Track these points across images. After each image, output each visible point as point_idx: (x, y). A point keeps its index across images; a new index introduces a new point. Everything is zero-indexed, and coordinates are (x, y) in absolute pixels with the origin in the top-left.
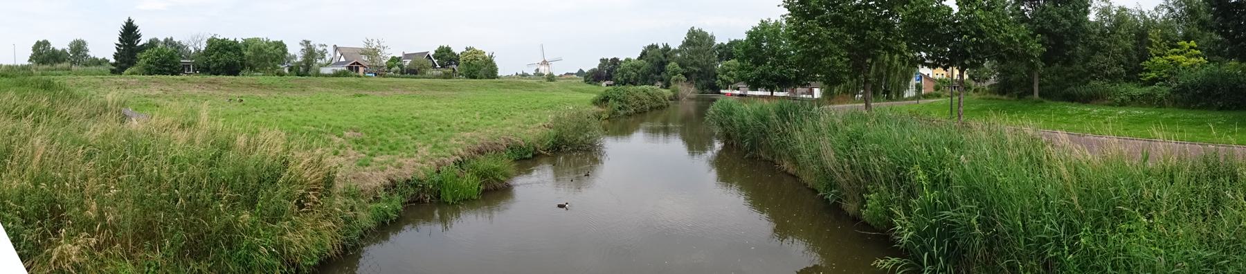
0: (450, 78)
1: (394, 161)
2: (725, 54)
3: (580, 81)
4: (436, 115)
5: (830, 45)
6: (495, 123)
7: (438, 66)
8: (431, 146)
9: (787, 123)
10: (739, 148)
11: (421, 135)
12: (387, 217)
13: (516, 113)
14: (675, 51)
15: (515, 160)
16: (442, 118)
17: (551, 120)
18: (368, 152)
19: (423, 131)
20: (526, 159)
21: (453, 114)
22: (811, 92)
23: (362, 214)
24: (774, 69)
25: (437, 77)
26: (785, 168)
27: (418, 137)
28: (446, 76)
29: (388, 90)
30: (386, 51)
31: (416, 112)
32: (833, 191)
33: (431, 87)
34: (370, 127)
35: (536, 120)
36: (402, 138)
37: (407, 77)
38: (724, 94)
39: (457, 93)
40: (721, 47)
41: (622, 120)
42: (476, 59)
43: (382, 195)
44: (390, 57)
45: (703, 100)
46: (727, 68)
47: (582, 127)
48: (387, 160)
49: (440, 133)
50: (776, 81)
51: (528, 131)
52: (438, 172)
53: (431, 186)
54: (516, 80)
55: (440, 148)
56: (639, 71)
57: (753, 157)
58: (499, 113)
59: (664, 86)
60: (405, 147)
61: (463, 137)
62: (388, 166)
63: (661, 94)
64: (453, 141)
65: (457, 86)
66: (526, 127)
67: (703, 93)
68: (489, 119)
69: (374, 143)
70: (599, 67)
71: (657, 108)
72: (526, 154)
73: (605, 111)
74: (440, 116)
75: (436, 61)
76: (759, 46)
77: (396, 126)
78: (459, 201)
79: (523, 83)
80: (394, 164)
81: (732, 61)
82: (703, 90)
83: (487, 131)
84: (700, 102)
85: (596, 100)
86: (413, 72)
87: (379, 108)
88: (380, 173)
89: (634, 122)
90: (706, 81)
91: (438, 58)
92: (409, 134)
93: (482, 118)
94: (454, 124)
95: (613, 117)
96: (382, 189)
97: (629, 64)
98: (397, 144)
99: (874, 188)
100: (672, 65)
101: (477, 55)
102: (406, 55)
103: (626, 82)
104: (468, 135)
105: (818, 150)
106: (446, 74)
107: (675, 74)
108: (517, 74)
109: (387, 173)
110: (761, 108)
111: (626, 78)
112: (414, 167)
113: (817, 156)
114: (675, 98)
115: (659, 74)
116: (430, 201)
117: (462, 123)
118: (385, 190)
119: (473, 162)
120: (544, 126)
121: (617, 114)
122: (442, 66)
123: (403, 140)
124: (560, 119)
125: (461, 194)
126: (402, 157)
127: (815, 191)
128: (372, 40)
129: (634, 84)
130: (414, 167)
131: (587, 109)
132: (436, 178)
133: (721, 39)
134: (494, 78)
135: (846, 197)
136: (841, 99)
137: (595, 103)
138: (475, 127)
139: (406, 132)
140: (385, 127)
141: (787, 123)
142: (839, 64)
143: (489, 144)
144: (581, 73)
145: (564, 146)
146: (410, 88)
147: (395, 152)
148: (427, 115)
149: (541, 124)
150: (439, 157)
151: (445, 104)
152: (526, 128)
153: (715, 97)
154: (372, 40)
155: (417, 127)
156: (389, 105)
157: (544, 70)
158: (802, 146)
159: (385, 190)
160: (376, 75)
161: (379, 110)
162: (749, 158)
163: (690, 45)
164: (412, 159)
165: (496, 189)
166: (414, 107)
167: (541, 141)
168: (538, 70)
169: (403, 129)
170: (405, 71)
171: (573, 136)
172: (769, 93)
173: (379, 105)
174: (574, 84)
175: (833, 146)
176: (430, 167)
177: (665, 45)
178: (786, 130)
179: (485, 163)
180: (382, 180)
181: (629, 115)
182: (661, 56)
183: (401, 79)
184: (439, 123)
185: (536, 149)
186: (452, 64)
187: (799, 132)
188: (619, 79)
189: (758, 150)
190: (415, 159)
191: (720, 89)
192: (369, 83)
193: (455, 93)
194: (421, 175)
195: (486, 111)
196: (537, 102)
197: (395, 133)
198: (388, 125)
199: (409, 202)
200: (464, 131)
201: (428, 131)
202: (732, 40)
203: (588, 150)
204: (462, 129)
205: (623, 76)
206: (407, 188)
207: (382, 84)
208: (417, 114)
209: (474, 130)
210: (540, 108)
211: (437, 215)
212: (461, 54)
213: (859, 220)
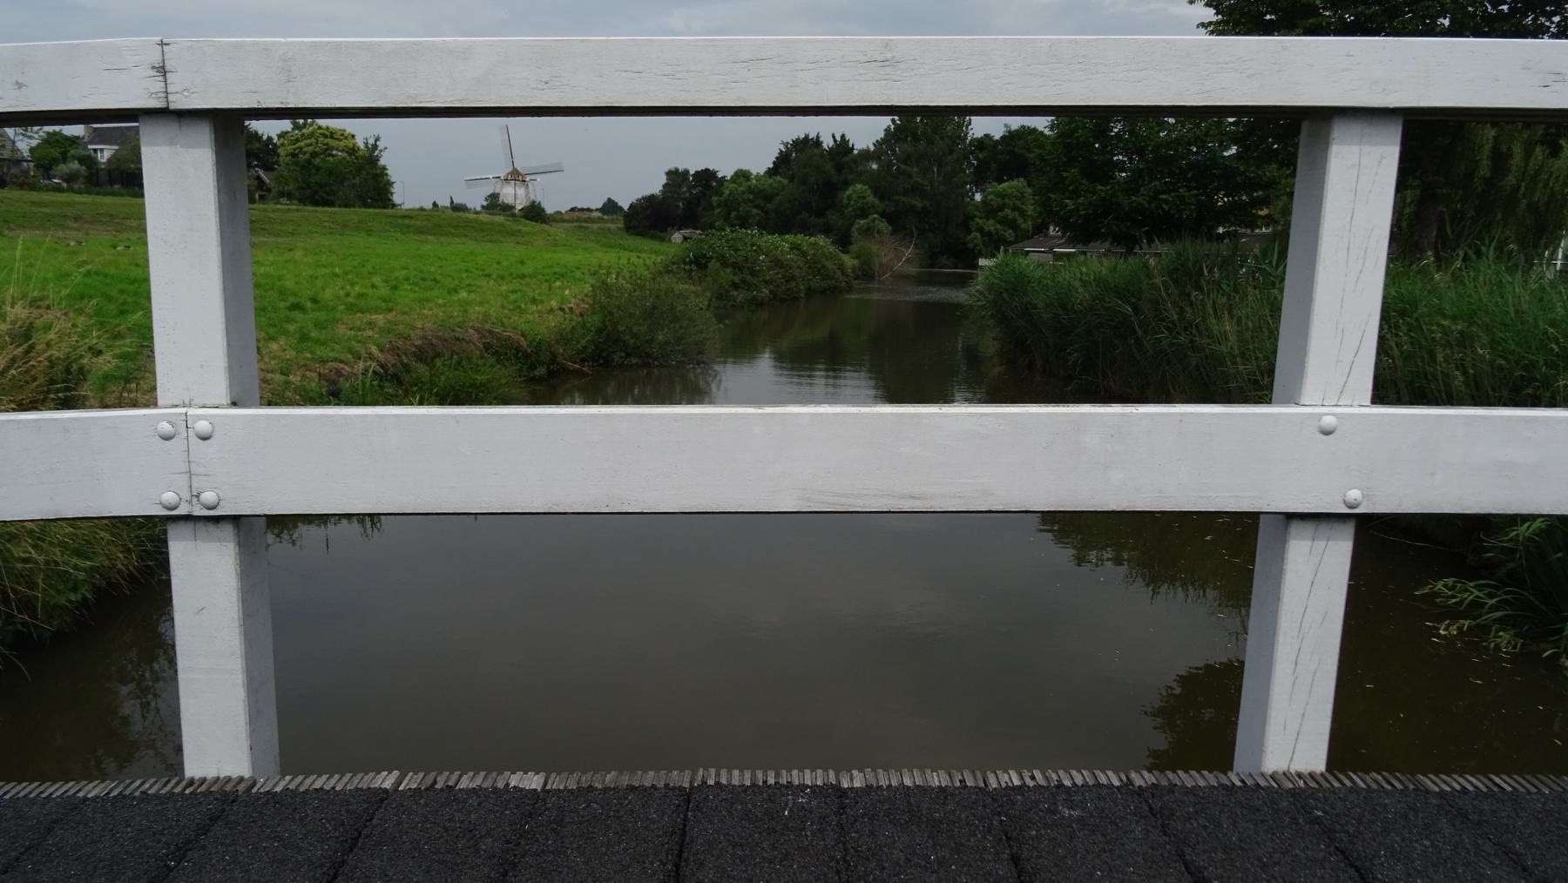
2: (994, 166)
3: (613, 226)
14: (866, 155)
37: (114, 194)
42: (328, 150)
46: (996, 202)
56: (769, 206)
67: (932, 266)
71: (823, 292)
107: (864, 215)
108: (435, 204)
114: (866, 273)
115: (821, 213)
143: (439, 338)
144: (610, 207)
149: (554, 303)
150: (323, 362)
157: (515, 196)
167: (563, 338)
177: (838, 139)
178: (1188, 315)
181: (757, 304)
182: (829, 166)
191: (976, 257)
207: (35, 209)
212: (280, 136)
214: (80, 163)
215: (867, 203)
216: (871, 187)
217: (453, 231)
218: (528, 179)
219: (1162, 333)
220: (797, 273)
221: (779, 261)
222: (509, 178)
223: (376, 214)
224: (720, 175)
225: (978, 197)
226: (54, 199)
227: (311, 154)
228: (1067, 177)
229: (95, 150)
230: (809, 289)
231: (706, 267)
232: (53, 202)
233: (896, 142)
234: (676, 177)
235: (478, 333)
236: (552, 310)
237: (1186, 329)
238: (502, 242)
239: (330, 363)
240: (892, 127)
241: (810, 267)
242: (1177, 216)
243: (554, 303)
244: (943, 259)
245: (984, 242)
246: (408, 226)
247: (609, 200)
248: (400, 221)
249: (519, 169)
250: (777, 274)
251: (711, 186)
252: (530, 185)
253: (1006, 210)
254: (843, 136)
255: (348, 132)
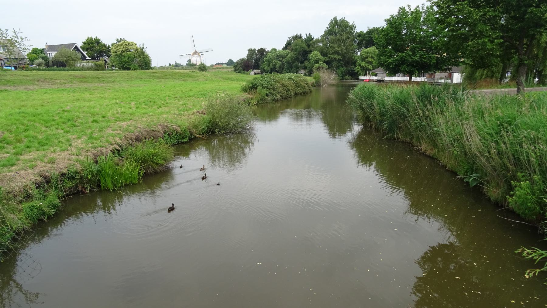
0: (102, 70)
1: (45, 156)
2: (364, 42)
3: (230, 70)
4: (89, 107)
5: (481, 27)
6: (151, 112)
7: (88, 58)
8: (86, 138)
9: (428, 106)
10: (377, 130)
11: (74, 128)
12: (44, 214)
13: (171, 101)
14: (318, 41)
15: (173, 145)
16: (96, 110)
17: (204, 107)
18: (13, 151)
19: (77, 124)
20: (183, 143)
21: (107, 105)
22: (450, 77)
23: (11, 216)
24: (414, 54)
25: (89, 69)
26: (423, 151)
27: (71, 130)
28: (98, 68)
29: (33, 84)
30: (25, 42)
31: (67, 105)
32: (474, 175)
33: (83, 79)
34: (12, 124)
35: (191, 107)
36: (52, 133)
37: (54, 70)
38: (363, 80)
39: (110, 84)
40: (359, 35)
41: (269, 106)
43: (35, 192)
44: (31, 49)
45: (342, 86)
47: (233, 112)
48: (36, 157)
49: (95, 124)
50: (415, 67)
51: (184, 117)
52: (96, 162)
53: (89, 177)
54: (169, 70)
55: (96, 139)
57: (391, 139)
58: (154, 102)
59: (307, 74)
60: (57, 141)
61: (120, 127)
62: (38, 163)
63: (305, 81)
64: (109, 131)
65: (110, 78)
66: (181, 114)
67: (342, 79)
68: (145, 108)
69: (20, 141)
70: (247, 56)
71: (301, 94)
72: (183, 138)
73: (254, 97)
74: (94, 108)
75: (85, 53)
76: (399, 33)
77: (44, 121)
78: (120, 187)
79: (176, 73)
80: (45, 160)
81: (370, 48)
82: (343, 77)
83: (144, 119)
84: (340, 88)
85: (246, 87)
86: (50, 65)
87: (23, 103)
88: (30, 171)
89: (280, 107)
90: (345, 68)
91: (87, 50)
92: (60, 127)
93: (137, 108)
94: (109, 114)
95: (261, 103)
96: (33, 186)
97: (275, 54)
98: (47, 139)
99: (523, 176)
100: (315, 54)
101: (130, 47)
102: (49, 46)
103: (273, 70)
104: (124, 124)
105: (460, 134)
106: (97, 66)
108: (170, 65)
109: (37, 170)
110: (401, 93)
111: (272, 67)
112: (69, 160)
113: (459, 139)
114: (318, 85)
116: (90, 191)
117: (118, 113)
118: (37, 188)
119: (131, 150)
120: (198, 112)
121: (265, 100)
122: (93, 58)
123: (54, 135)
124: (212, 105)
125: (122, 180)
126: (54, 152)
127: (455, 174)
128: (7, 30)
129: (280, 71)
130: (69, 160)
131: (237, 96)
132: (95, 168)
133: (362, 27)
134: (148, 69)
135: (488, 182)
136: (484, 84)
137: (244, 90)
138: (131, 117)
139: (57, 126)
140: (31, 123)
141: (428, 106)
142: (489, 46)
143: (146, 131)
144: (230, 62)
145: (217, 130)
146: (58, 81)
147: (46, 147)
148: (80, 108)
149: (195, 110)
150: (96, 147)
151: (99, 95)
152: (181, 115)
153: (356, 83)
154: (7, 30)
155: (69, 120)
156: (34, 100)
157: (196, 61)
158: (442, 129)
159: (37, 188)
160: (16, 68)
161: (23, 106)
162: (387, 139)
163: (332, 34)
164: (66, 153)
165: (156, 173)
166: (64, 100)
167: (196, 126)
168: (190, 60)
169: (53, 123)
170: (51, 64)
171: (226, 120)
172: (407, 79)
173: (22, 101)
174: (225, 73)
175: (479, 131)
176: (87, 158)
178: (427, 113)
179: (143, 149)
180: (33, 178)
181: (276, 101)
182: (304, 45)
183: (47, 72)
184: (93, 114)
185: (191, 134)
186: (103, 56)
187: (440, 116)
188: (265, 68)
189: (397, 132)
190: (69, 152)
191: (358, 76)
192: (8, 78)
193: (108, 85)
194: (78, 167)
195: (142, 100)
196: (191, 90)
197: (44, 129)
198: (34, 121)
199: (67, 195)
200: (120, 121)
201: (82, 123)
202: (372, 28)
203: (240, 133)
204: (118, 120)
205: (269, 66)
206: (62, 181)
207: (24, 78)
208: (68, 107)
209: (130, 120)
210: (194, 96)
211: (100, 203)
212: (112, 45)
213: (502, 206)
214: (42, 59)
215: (318, 58)
216: (320, 52)
217: (170, 77)
218: (200, 54)
219: (417, 120)
220: (290, 88)
221: (284, 84)
222: (194, 54)
223: (144, 72)
224: (266, 50)
225: (359, 54)
226: (31, 74)
227: (121, 52)
228: (387, 51)
229: (49, 53)
230: (296, 93)
231: (257, 89)
232: (31, 75)
233: (328, 36)
234: (251, 52)
235: (162, 127)
236: (194, 113)
237: (426, 119)
238: (187, 80)
239: (98, 148)
240: (327, 30)
241: (296, 85)
242: (429, 63)
243: (195, 110)
244: (347, 77)
245: (361, 70)
246: (155, 76)
247: (230, 59)
248: (152, 74)
249: (198, 51)
250: (283, 89)
251: (264, 54)
252: (201, 56)
253: (369, 58)
254: (310, 34)
255: (134, 43)
